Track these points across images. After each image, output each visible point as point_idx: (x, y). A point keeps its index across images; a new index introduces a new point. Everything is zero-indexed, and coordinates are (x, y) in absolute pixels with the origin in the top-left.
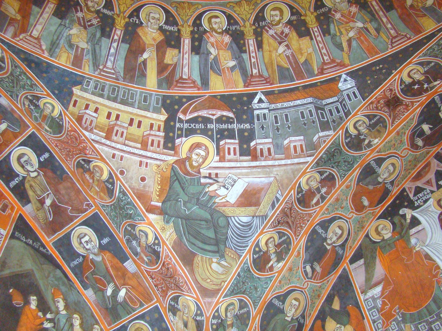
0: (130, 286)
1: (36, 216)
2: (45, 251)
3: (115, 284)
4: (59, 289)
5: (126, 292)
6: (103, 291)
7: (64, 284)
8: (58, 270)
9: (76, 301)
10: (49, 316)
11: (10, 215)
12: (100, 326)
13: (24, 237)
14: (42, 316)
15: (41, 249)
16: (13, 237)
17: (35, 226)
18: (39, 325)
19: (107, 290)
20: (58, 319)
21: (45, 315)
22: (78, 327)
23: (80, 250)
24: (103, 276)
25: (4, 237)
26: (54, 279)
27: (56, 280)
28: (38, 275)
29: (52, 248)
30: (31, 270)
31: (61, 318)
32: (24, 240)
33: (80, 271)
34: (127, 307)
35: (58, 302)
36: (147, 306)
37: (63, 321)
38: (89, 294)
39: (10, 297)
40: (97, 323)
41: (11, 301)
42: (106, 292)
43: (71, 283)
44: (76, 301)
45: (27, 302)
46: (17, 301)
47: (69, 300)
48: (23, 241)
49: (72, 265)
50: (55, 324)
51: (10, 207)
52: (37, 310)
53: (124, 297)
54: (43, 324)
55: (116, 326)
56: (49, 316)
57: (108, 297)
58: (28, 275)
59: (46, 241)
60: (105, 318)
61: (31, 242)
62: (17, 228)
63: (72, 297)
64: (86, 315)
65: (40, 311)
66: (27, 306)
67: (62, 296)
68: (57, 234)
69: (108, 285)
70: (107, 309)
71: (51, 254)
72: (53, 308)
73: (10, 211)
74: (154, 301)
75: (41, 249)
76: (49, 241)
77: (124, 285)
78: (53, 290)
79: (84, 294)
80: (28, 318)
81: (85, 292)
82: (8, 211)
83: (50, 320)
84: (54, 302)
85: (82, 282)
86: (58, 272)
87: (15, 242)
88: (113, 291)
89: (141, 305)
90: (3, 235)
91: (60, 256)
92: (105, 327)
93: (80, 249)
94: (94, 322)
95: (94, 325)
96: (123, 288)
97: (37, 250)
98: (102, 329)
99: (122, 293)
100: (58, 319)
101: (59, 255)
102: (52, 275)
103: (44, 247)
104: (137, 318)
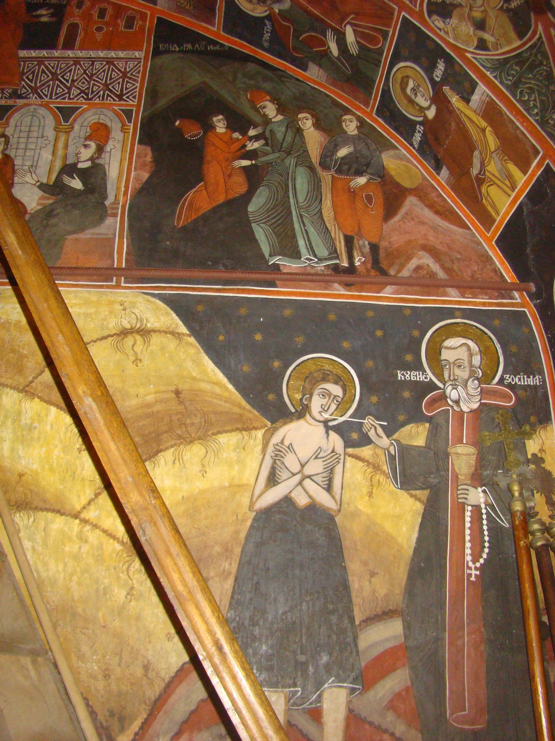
0: (351, 14)
1: (177, 5)
2: (218, 48)
3: (333, 29)
4: (259, 89)
5: (354, 30)
6: (326, 54)
7: (266, 79)
8: (249, 63)
9: (298, 95)
10: (252, 132)
11: (142, 28)
12: (354, 114)
13: (175, 45)
14: (241, 137)
15: (211, 48)
16: (157, 53)
17: (189, 22)
18: (238, 151)
19: (329, 48)
20: (271, 131)
21: (244, 132)
22: (312, 129)
23: (258, 11)
24: (310, 29)
25: (142, 60)
26: (245, 80)
27: (250, 79)
28: (215, 85)
29: (228, 38)
30: (202, 83)
31: (276, 128)
32: (177, 49)
33: (278, 47)
34: (369, 55)
35: (264, 108)
36: (391, 30)
37: (280, 132)
38: (314, 74)
39: (179, 131)
40: (347, 111)
41: (182, 135)
42: (331, 52)
43: (280, 73)
44: (298, 95)
45: (209, 128)
46: (192, 132)
47: (283, 98)
48: (175, 51)
49: (266, 45)
50: (266, 139)
51: (138, 16)
52: (229, 132)
53: (356, 40)
54: (245, 146)
55: (375, 99)
56: (252, 132)
57: (338, 58)
58: (200, 91)
59: (213, 33)
60: (356, 98)
61: (189, 46)
62: (159, 39)
63: (288, 92)
64: (321, 108)
65: (235, 131)
66: (210, 134)
67: (268, 98)
68: (217, 11)
69: (325, 36)
70: (348, 80)
71: (230, 48)
72: (257, 119)
73: (140, 23)
74: (396, 13)
75: (211, 48)
76: (214, 30)
77: (343, 19)
78: (249, 96)
79: (310, 79)
80: (217, 147)
81: (307, 74)
82: (138, 23)
83: (257, 138)
84: (257, 110)
85: (293, 61)
86: (251, 67)
87: (166, 59)
88: (337, 44)
89: (385, 34)
90: (141, 59)
91: (244, 43)
92: (364, 112)
93: (256, 10)
94: (341, 112)
95: (342, 116)
96: (345, 26)
97: (205, 53)
98: (359, 116)
99: (350, 36)
100: (271, 131)
101: (242, 41)
102: (240, 75)
103: (215, 43)
104: (392, 65)
